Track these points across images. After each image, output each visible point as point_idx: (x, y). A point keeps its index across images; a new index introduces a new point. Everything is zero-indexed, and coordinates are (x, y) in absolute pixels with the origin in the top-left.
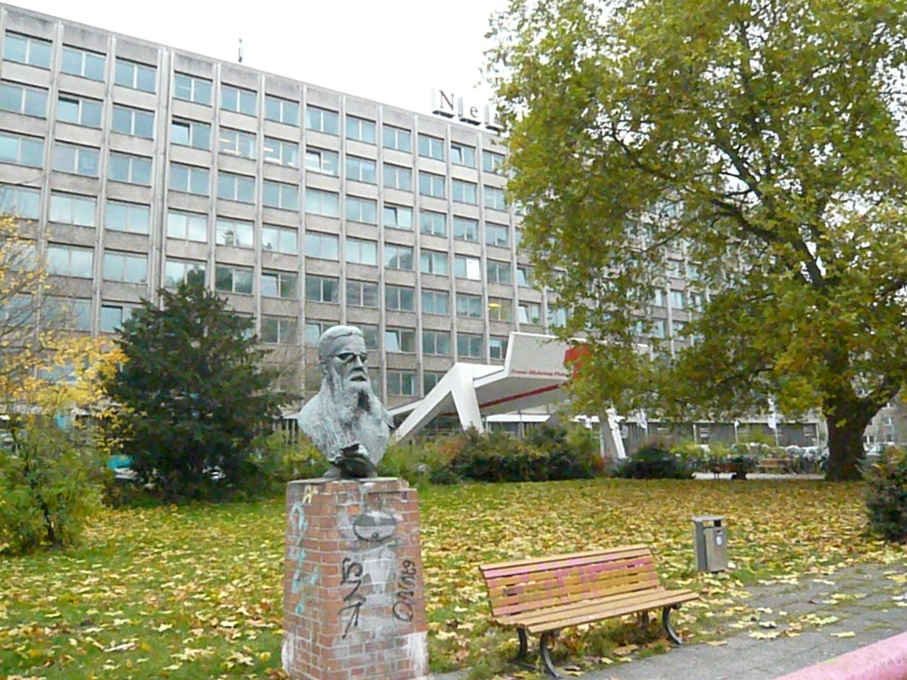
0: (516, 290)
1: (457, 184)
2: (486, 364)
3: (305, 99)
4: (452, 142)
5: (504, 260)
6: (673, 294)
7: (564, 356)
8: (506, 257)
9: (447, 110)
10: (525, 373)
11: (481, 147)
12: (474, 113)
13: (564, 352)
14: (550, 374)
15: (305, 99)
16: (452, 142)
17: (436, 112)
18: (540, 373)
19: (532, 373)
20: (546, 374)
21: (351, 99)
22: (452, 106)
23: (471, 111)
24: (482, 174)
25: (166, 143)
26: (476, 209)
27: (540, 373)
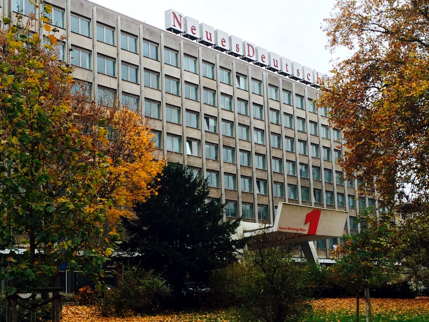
0: (205, 161)
1: (102, 59)
2: (255, 222)
3: (96, 18)
4: (236, 72)
5: (248, 150)
6: (208, 146)
7: (304, 218)
8: (215, 140)
9: (177, 28)
10: (285, 229)
11: (120, 28)
12: (194, 31)
13: (305, 215)
14: (297, 230)
15: (96, 18)
16: (236, 72)
17: (170, 29)
18: (292, 229)
19: (289, 229)
20: (295, 229)
21: (102, 10)
22: (180, 25)
23: (262, 58)
24: (202, 78)
25: (268, 122)
26: (292, 132)
27: (292, 229)
